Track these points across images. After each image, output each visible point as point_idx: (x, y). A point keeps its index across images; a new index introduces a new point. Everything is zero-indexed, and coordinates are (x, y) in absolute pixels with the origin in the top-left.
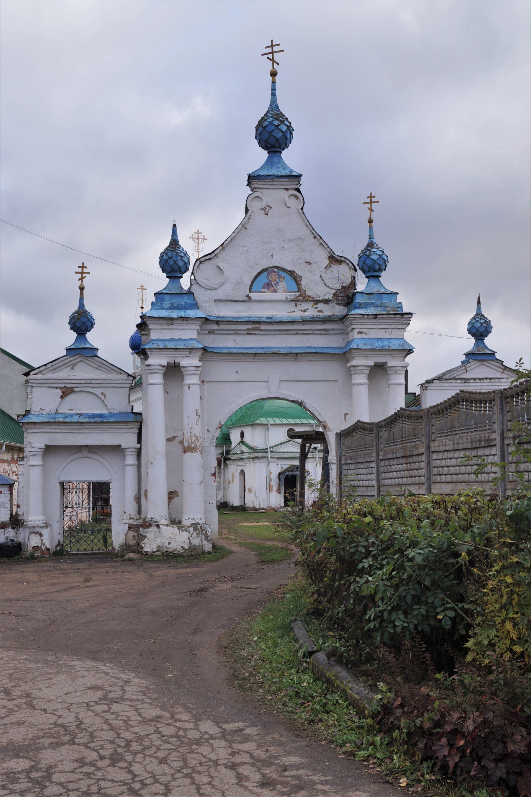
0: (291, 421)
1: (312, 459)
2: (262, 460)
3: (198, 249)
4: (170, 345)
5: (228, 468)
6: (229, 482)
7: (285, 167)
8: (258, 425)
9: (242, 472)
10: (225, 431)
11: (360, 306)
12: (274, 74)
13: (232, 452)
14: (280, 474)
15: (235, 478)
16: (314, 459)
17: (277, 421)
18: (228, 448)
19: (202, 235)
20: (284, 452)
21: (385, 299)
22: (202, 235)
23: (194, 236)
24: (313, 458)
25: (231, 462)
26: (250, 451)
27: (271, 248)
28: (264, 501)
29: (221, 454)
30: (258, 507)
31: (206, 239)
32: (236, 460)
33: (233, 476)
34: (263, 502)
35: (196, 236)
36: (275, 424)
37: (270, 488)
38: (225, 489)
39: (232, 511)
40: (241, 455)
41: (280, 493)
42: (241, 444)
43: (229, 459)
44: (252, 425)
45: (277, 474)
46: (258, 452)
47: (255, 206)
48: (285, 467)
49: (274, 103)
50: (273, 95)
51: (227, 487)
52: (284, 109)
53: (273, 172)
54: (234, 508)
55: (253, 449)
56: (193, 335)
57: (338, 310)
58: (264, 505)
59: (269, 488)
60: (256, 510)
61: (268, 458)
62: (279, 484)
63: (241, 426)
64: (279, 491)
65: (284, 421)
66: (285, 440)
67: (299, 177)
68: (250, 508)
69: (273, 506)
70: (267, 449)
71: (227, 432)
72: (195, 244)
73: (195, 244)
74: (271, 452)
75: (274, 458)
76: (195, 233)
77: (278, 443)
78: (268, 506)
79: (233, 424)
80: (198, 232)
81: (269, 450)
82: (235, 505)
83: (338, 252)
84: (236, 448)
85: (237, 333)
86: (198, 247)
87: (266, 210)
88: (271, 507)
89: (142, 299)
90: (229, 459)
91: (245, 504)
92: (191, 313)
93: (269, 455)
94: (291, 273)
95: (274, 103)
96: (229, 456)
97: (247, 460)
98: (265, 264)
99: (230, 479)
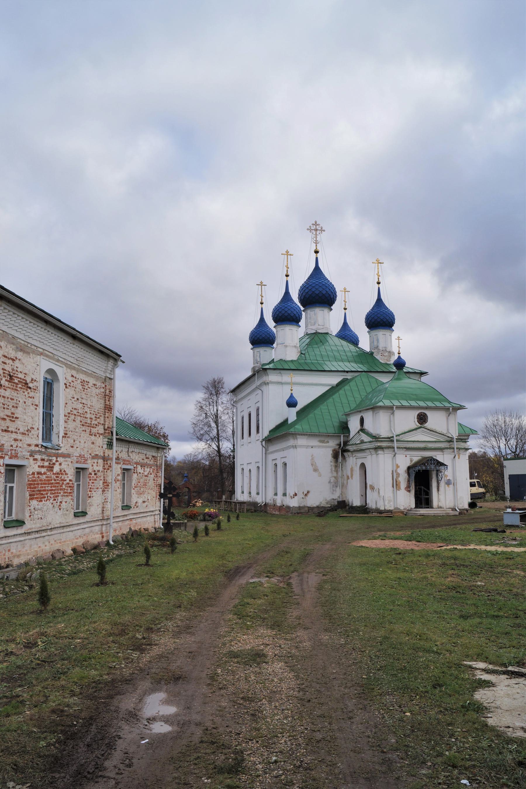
0: (422, 404)
1: (449, 450)
2: (386, 451)
3: (316, 241)
5: (346, 461)
6: (348, 478)
8: (381, 407)
9: (363, 466)
10: (343, 418)
13: (351, 443)
14: (409, 468)
15: (354, 473)
16: (452, 450)
17: (405, 403)
18: (346, 439)
19: (320, 226)
20: (413, 442)
22: (320, 226)
23: (312, 228)
24: (450, 448)
25: (349, 454)
26: (371, 440)
27: (359, 753)
28: (390, 501)
29: (338, 445)
30: (382, 508)
31: (324, 231)
32: (355, 451)
33: (352, 470)
34: (388, 503)
35: (313, 227)
36: (402, 407)
37: (397, 485)
38: (343, 486)
39: (350, 513)
40: (361, 445)
41: (409, 491)
42: (360, 433)
43: (348, 451)
44: (374, 408)
45: (406, 468)
46: (382, 441)
48: (416, 459)
51: (345, 482)
54: (354, 510)
55: (376, 438)
58: (390, 506)
59: (396, 485)
60: (380, 512)
61: (394, 448)
62: (409, 481)
63: (360, 411)
64: (408, 488)
65: (413, 403)
66: (414, 426)
68: (372, 509)
69: (402, 508)
70: (393, 437)
71: (345, 420)
72: (313, 236)
73: (313, 236)
74: (397, 441)
75: (402, 448)
76: (313, 224)
77: (406, 430)
78: (395, 509)
79: (351, 410)
80: (316, 224)
81: (395, 438)
82: (354, 505)
84: (355, 437)
86: (316, 239)
88: (399, 509)
89: (262, 297)
90: (348, 451)
91: (366, 503)
93: (396, 445)
96: (348, 448)
97: (368, 451)
99: (349, 474)
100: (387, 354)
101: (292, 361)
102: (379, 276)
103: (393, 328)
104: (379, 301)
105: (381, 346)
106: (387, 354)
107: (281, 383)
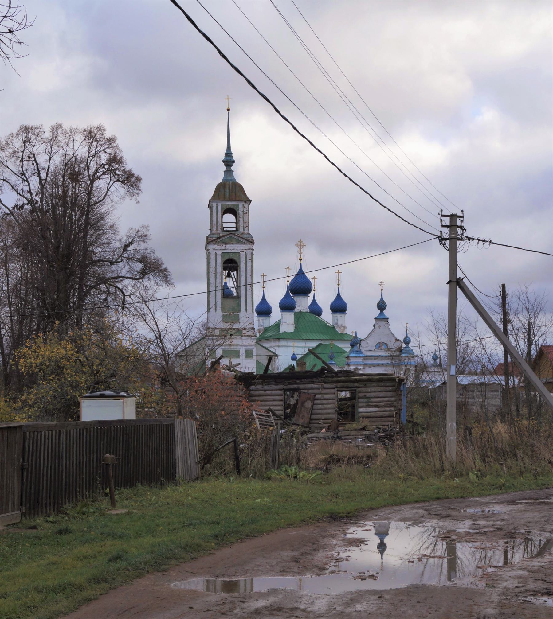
3: (301, 252)
4: (356, 363)
7: (384, 315)
11: (403, 353)
12: (382, 290)
21: (410, 352)
47: (377, 326)
49: (382, 298)
50: (382, 296)
52: (385, 299)
53: (382, 317)
56: (361, 361)
57: (398, 353)
67: (388, 319)
80: (300, 241)
83: (398, 338)
85: (371, 359)
87: (379, 327)
92: (361, 355)
94: (386, 344)
95: (382, 298)
98: (379, 341)
100: (342, 328)
101: (291, 333)
102: (339, 280)
103: (309, 294)
104: (339, 296)
105: (339, 323)
106: (342, 328)
107: (287, 346)
